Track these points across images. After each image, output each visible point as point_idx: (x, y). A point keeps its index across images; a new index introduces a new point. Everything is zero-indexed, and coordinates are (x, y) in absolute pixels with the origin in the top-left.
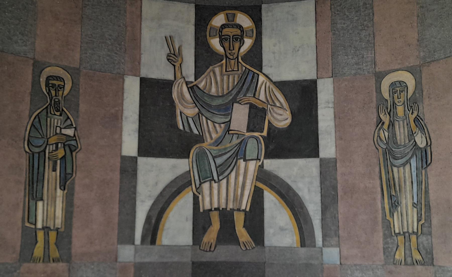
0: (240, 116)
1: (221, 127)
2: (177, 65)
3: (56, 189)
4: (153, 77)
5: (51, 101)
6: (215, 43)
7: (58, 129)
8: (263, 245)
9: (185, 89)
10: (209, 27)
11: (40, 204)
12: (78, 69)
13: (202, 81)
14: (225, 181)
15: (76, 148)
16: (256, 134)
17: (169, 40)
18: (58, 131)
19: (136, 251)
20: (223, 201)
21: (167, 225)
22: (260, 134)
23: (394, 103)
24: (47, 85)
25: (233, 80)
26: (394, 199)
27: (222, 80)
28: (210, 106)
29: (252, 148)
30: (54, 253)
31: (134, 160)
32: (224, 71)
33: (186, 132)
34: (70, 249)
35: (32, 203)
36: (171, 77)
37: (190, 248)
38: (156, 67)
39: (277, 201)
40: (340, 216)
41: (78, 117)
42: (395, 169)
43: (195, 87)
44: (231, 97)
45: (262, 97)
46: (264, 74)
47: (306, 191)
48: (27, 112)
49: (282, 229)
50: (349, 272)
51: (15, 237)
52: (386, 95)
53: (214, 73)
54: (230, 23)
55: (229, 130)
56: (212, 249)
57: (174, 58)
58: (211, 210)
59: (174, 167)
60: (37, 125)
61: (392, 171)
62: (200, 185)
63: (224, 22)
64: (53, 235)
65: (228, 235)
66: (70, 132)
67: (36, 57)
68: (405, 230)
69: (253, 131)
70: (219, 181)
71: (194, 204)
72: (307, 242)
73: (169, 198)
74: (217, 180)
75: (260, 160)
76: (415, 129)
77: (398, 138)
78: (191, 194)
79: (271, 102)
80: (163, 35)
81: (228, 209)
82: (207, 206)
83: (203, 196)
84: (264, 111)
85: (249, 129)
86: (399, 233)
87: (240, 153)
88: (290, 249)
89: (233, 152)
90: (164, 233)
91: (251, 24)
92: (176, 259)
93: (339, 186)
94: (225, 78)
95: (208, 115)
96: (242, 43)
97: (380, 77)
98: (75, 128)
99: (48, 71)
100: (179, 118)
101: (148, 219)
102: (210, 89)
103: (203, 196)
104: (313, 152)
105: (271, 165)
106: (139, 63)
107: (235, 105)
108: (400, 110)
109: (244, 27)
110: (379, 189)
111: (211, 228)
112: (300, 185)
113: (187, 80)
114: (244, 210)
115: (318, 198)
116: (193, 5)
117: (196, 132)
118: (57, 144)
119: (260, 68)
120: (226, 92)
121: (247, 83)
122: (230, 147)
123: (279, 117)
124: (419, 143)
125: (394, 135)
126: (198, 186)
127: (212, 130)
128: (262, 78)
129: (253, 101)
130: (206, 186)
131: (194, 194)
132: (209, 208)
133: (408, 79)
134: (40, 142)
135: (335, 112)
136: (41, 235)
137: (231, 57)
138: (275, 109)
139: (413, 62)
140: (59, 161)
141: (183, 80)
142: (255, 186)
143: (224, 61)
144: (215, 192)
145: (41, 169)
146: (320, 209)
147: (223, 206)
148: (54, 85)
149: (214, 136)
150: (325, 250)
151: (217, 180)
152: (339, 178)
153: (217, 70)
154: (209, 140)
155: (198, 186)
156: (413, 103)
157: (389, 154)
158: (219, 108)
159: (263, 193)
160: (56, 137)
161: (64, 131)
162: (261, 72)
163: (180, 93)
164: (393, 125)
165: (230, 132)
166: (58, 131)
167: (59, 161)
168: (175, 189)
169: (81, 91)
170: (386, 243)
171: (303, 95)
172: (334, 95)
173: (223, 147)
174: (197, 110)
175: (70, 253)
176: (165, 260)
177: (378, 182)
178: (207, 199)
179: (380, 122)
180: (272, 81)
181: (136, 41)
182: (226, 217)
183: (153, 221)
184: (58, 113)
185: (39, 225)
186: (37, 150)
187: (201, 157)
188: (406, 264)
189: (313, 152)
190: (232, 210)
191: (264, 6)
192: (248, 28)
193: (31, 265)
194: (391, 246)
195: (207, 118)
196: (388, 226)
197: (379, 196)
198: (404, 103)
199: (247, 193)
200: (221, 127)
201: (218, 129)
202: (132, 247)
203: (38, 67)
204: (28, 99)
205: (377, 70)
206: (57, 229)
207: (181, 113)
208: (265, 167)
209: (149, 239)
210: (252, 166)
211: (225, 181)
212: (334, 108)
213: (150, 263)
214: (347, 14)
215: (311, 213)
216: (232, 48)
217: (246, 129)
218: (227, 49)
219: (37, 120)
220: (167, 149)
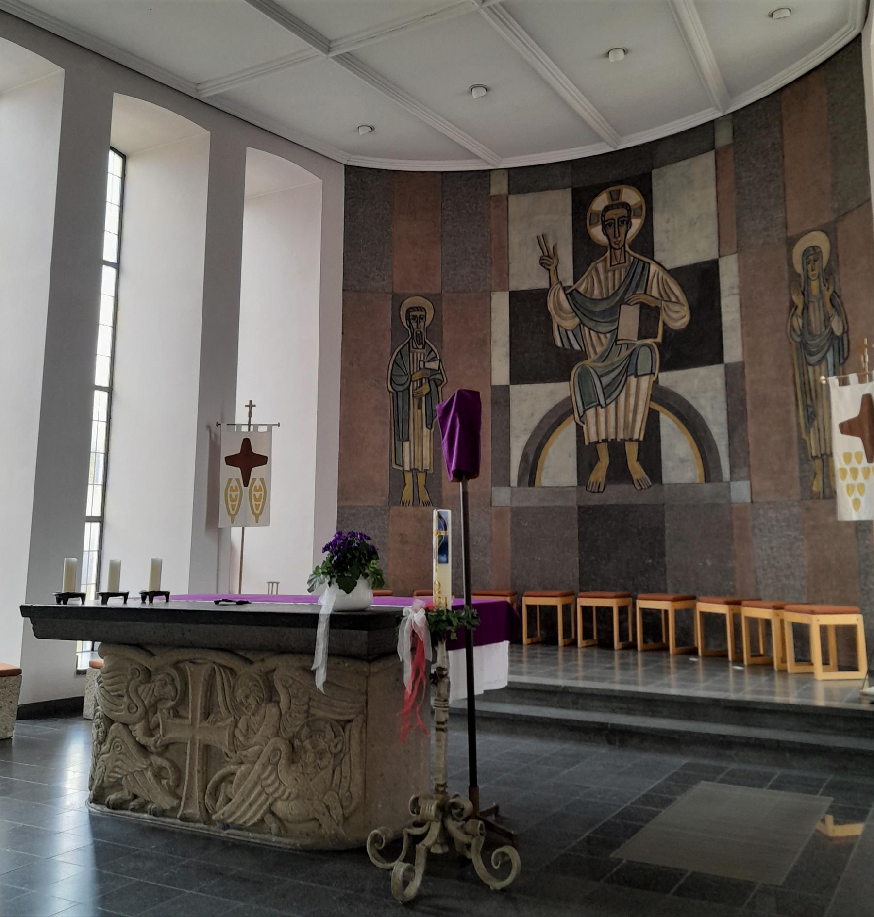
0: (629, 320)
1: (606, 337)
2: (552, 268)
3: (422, 428)
4: (524, 288)
5: (412, 334)
6: (597, 232)
7: (422, 363)
8: (661, 482)
9: (562, 296)
10: (589, 213)
11: (406, 444)
12: (440, 294)
13: (582, 283)
14: (613, 405)
15: (442, 382)
16: (649, 341)
17: (542, 240)
18: (422, 366)
19: (513, 494)
20: (612, 430)
21: (546, 463)
22: (652, 340)
23: (808, 277)
24: (408, 318)
25: (620, 275)
26: (810, 410)
27: (607, 279)
28: (592, 312)
29: (644, 361)
30: (424, 496)
31: (506, 389)
32: (609, 264)
33: (566, 349)
34: (440, 492)
35: (399, 444)
36: (545, 284)
37: (575, 489)
38: (526, 274)
39: (675, 426)
40: (750, 439)
41: (442, 348)
42: (810, 369)
43: (574, 292)
44: (618, 298)
45: (655, 292)
46: (656, 262)
47: (709, 409)
48: (389, 350)
49: (682, 461)
50: (761, 512)
51: (382, 479)
52: (799, 268)
53: (597, 271)
54: (616, 203)
55: (616, 340)
56: (601, 490)
57: (548, 260)
58: (598, 442)
59: (552, 393)
60: (400, 362)
61: (808, 371)
62: (584, 412)
63: (607, 203)
64: (421, 477)
65: (619, 472)
66: (434, 365)
67: (395, 291)
68: (823, 452)
69: (646, 338)
70: (607, 405)
71: (578, 436)
72: (713, 476)
73: (548, 431)
74: (604, 405)
75: (654, 374)
76: (831, 310)
77: (813, 325)
78: (573, 425)
79: (666, 298)
80: (534, 235)
81: (618, 440)
82: (594, 438)
83: (587, 426)
84: (658, 310)
85: (641, 336)
86: (817, 456)
87: (630, 369)
88: (692, 485)
89: (621, 367)
90: (544, 473)
91: (639, 199)
92: (559, 503)
93: (748, 398)
94: (610, 274)
95: (591, 324)
96: (629, 225)
97: (791, 243)
98: (440, 361)
99: (408, 303)
100: (556, 333)
101: (525, 456)
102: (593, 290)
103: (587, 426)
104: (716, 357)
105: (668, 379)
106: (508, 275)
107: (622, 306)
108: (814, 285)
109: (631, 204)
110: (793, 399)
111: (599, 464)
112: (702, 402)
113: (564, 285)
114: (638, 440)
115: (723, 417)
116: (569, 190)
117: (577, 347)
118: (421, 380)
119: (650, 254)
120: (611, 292)
121: (636, 278)
122: (618, 361)
123: (675, 316)
124: (835, 329)
125: (809, 324)
126: (581, 414)
127: (596, 343)
128: (653, 268)
129: (644, 299)
130: (591, 413)
131: (577, 424)
132: (596, 440)
133: (820, 240)
134: (404, 379)
135: (740, 301)
136: (409, 477)
137: (616, 247)
138: (670, 305)
139: (827, 217)
140: (424, 399)
141: (559, 286)
142: (650, 408)
143: (608, 254)
144: (602, 419)
145: (406, 407)
146: (726, 431)
147: (612, 436)
148: (415, 317)
149: (599, 350)
150: (734, 485)
151: (604, 405)
152: (747, 388)
153: (600, 266)
154: (593, 355)
155: (581, 414)
156: (829, 274)
157: (804, 349)
158: (603, 313)
159: (659, 416)
160: (420, 372)
161: (427, 365)
162: (653, 260)
163: (558, 301)
164: (808, 308)
165: (618, 342)
166: (422, 366)
167: (424, 399)
168: (555, 419)
169: (444, 318)
170: (802, 471)
171: (701, 282)
172: (740, 277)
173: (610, 362)
174: (577, 320)
175: (441, 496)
176: (546, 504)
177: (791, 389)
178: (593, 429)
179: (793, 305)
180: (664, 269)
181: (503, 250)
182: (616, 448)
183: (531, 459)
184: (421, 347)
185: (407, 468)
186: (401, 388)
187: (584, 376)
188: (824, 498)
189: (716, 357)
190: (624, 440)
191: (654, 172)
192: (636, 204)
193: (401, 508)
194: (808, 474)
195: (590, 329)
196: (803, 446)
197: (794, 407)
198: (818, 277)
199: (639, 417)
200: (606, 337)
201: (603, 340)
202: (508, 489)
203: (397, 300)
204: (388, 336)
205: (789, 234)
206: (426, 471)
207: (558, 326)
208: (661, 383)
209: (527, 479)
210: (645, 383)
211: (613, 405)
212: (740, 294)
213: (528, 508)
214: (754, 162)
215: (716, 438)
216: (617, 235)
217: (636, 336)
218: (612, 237)
219: (399, 356)
220: (543, 372)
